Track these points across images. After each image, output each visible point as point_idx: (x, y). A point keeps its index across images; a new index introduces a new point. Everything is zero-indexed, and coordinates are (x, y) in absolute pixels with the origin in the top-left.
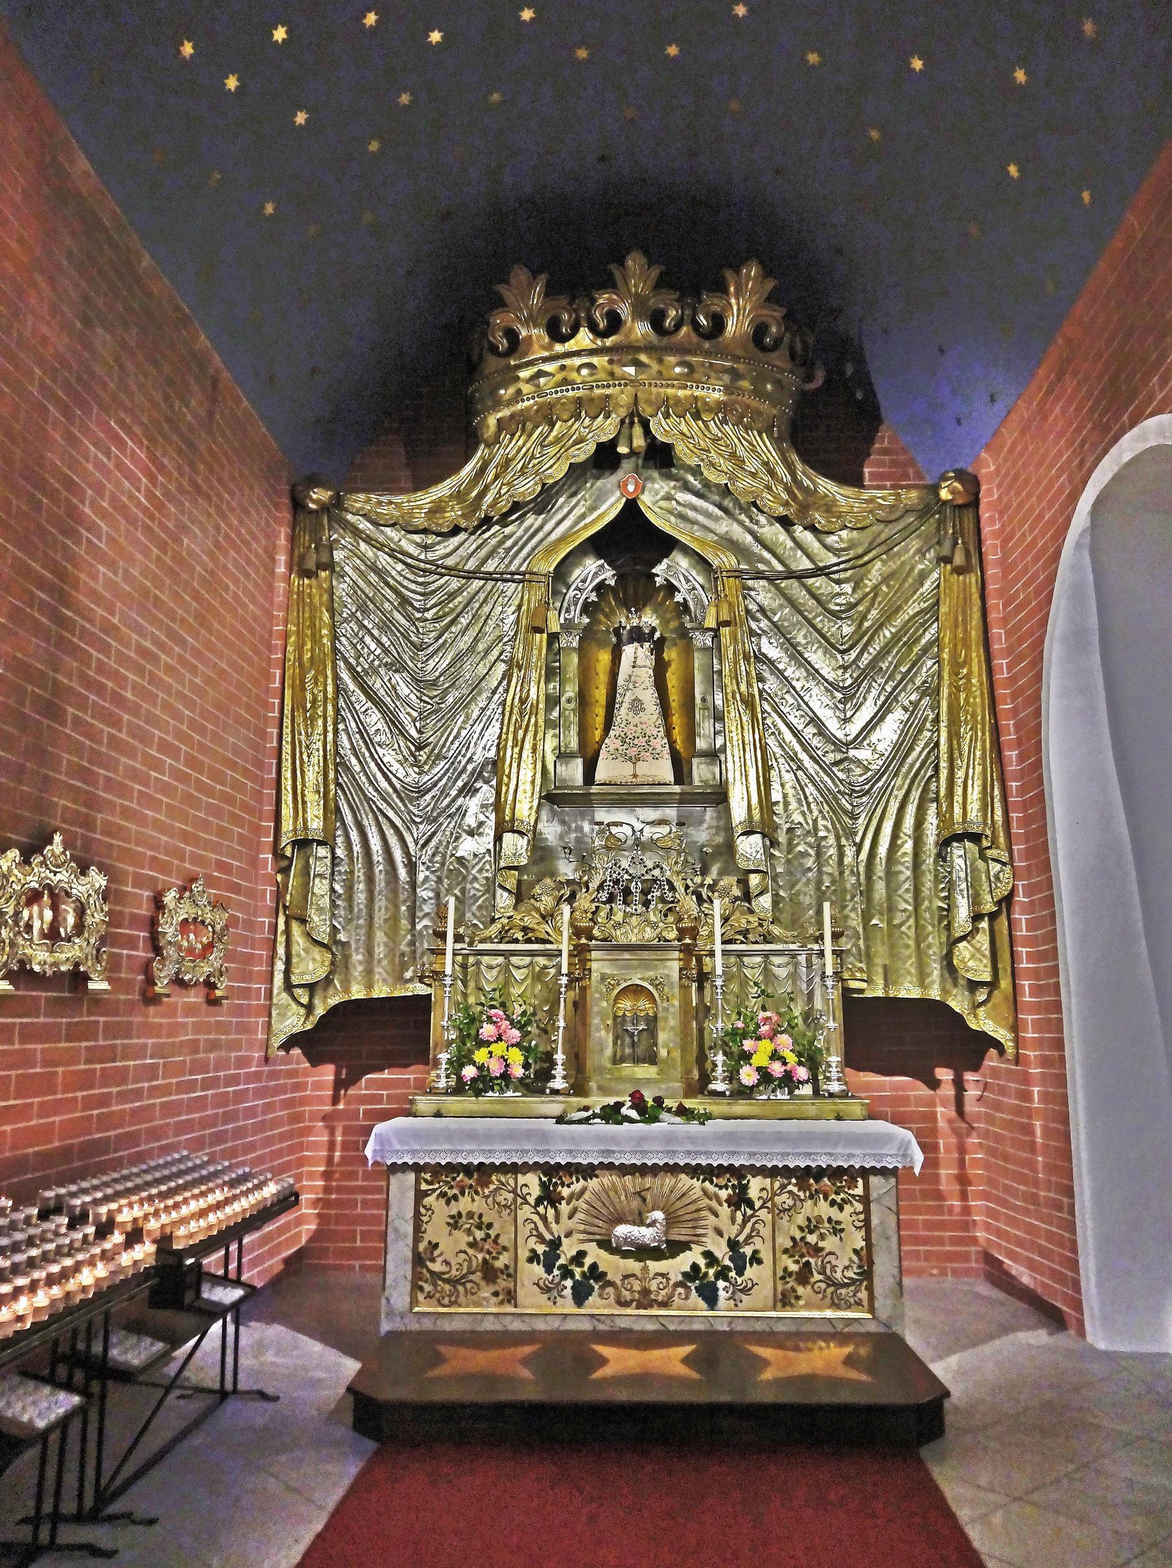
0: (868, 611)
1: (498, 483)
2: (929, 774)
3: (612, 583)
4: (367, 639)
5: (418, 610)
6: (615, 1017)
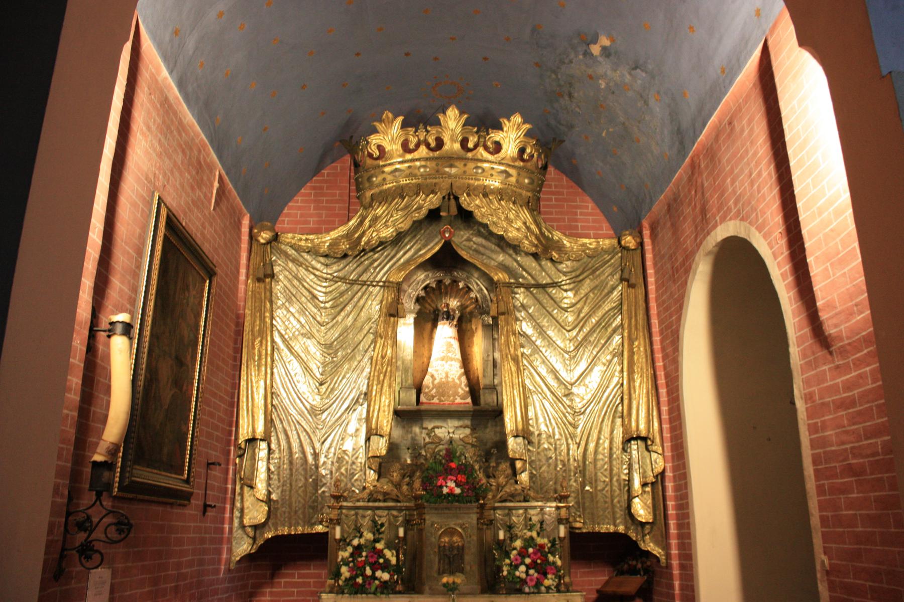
0: (583, 308)
1: (371, 230)
2: (617, 403)
3: (434, 286)
4: (292, 319)
5: (322, 302)
6: (439, 547)
